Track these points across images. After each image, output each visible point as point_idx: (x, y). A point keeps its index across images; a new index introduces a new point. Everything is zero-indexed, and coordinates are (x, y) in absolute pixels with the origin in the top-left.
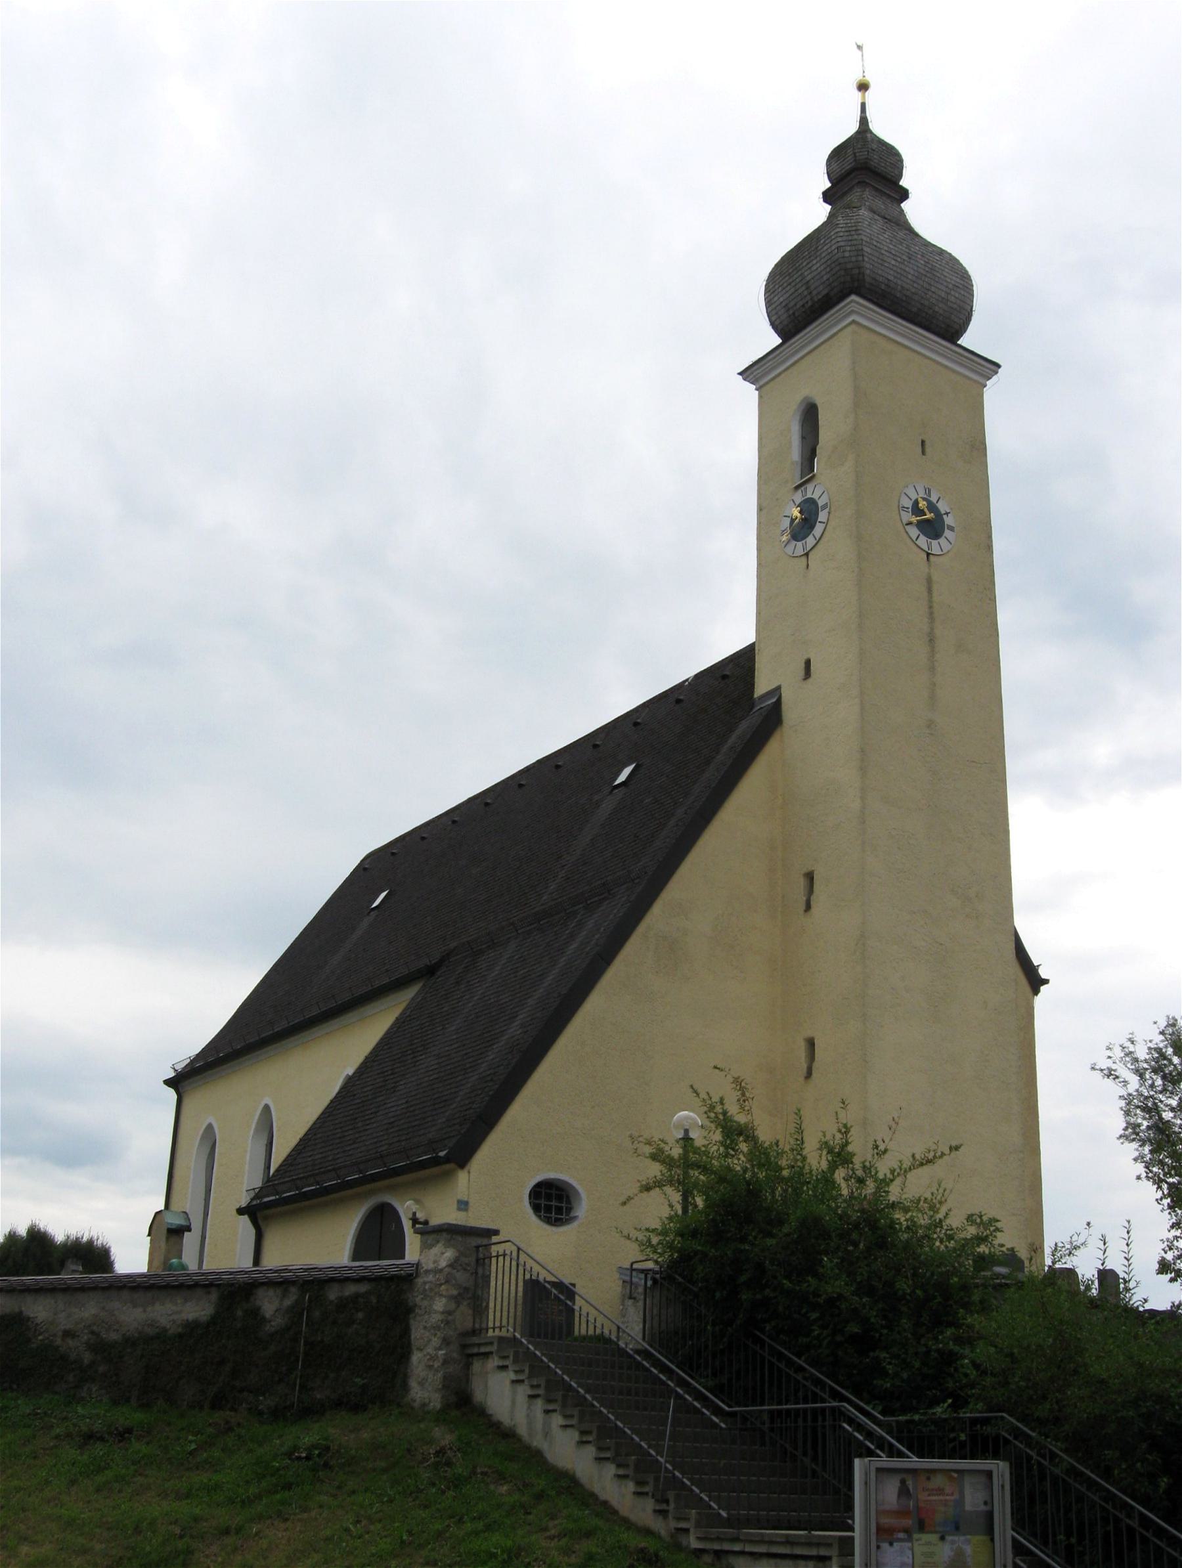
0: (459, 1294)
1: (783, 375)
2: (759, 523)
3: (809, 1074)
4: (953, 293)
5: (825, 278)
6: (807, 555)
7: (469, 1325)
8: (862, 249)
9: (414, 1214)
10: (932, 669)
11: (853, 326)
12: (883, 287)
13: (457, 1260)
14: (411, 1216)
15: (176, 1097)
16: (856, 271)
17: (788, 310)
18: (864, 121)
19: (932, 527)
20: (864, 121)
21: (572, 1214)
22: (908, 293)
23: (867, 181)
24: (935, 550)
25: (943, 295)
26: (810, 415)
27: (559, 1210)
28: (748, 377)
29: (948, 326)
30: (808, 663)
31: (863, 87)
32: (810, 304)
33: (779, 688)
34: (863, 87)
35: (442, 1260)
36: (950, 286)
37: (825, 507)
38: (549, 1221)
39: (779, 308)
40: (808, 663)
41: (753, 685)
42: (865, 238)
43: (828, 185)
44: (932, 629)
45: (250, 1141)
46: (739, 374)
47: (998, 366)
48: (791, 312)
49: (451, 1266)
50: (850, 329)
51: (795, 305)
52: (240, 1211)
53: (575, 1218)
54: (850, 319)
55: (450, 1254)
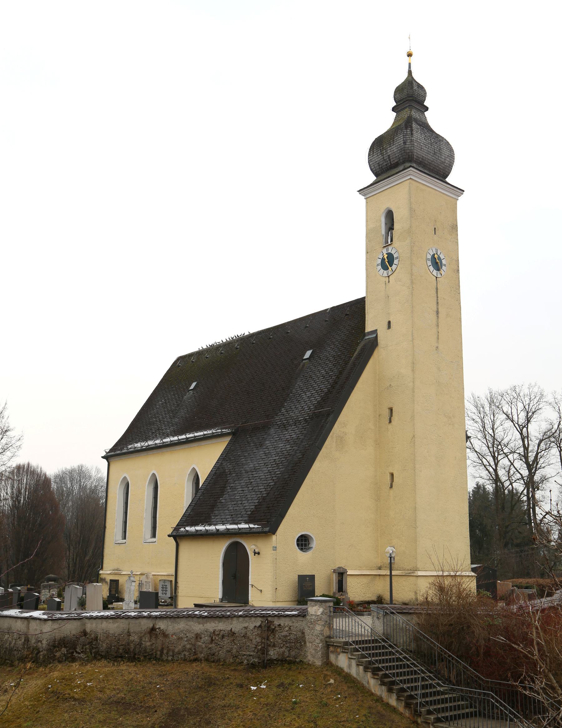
0: (325, 624)
1: (377, 195)
2: (367, 258)
3: (391, 487)
4: (447, 159)
5: (397, 155)
6: (389, 277)
7: (328, 634)
8: (414, 144)
9: (255, 550)
10: (438, 326)
11: (410, 180)
12: (421, 160)
13: (323, 611)
14: (253, 551)
15: (107, 463)
16: (411, 154)
17: (379, 165)
18: (410, 72)
19: (437, 264)
20: (410, 72)
21: (310, 546)
22: (430, 161)
23: (413, 105)
24: (439, 276)
25: (443, 160)
26: (390, 215)
27: (305, 545)
28: (362, 193)
29: (444, 173)
30: (389, 323)
31: (410, 55)
32: (389, 164)
33: (376, 330)
34: (410, 55)
35: (318, 612)
36: (446, 156)
37: (397, 258)
38: (302, 549)
39: (375, 164)
40: (389, 323)
41: (365, 329)
42: (415, 139)
43: (395, 104)
44: (438, 309)
45: (146, 487)
46: (358, 191)
47: (463, 191)
48: (381, 166)
49: (322, 614)
50: (408, 181)
51: (383, 164)
52: (169, 536)
53: (312, 548)
54: (409, 177)
55: (321, 610)
